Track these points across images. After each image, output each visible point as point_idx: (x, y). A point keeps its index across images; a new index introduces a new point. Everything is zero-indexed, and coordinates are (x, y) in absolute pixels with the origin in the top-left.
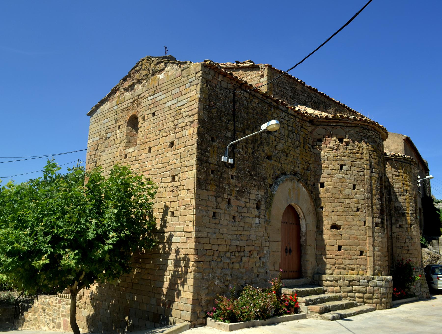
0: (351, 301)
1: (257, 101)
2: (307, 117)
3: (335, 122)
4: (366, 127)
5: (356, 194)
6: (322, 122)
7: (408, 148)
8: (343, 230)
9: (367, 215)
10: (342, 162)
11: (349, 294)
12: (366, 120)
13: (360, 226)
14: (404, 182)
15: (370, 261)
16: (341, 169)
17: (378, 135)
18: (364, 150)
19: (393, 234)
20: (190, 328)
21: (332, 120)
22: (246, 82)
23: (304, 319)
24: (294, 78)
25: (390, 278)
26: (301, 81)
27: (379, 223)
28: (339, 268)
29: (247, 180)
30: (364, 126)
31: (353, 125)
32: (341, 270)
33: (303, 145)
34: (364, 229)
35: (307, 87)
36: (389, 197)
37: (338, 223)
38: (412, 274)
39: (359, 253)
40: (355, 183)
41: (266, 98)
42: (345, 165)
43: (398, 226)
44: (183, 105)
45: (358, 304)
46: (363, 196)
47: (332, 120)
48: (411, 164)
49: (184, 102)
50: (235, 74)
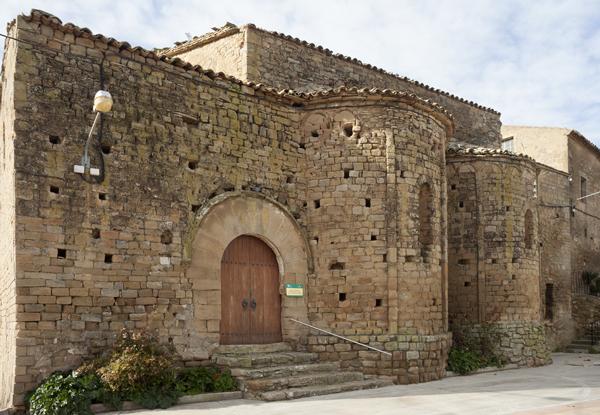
1: (161, 75)
6: (318, 103)
16: (347, 176)
29: (137, 201)
31: (368, 103)
33: (277, 143)
37: (340, 260)
40: (369, 197)
42: (353, 169)
43: (490, 261)
48: (519, 165)
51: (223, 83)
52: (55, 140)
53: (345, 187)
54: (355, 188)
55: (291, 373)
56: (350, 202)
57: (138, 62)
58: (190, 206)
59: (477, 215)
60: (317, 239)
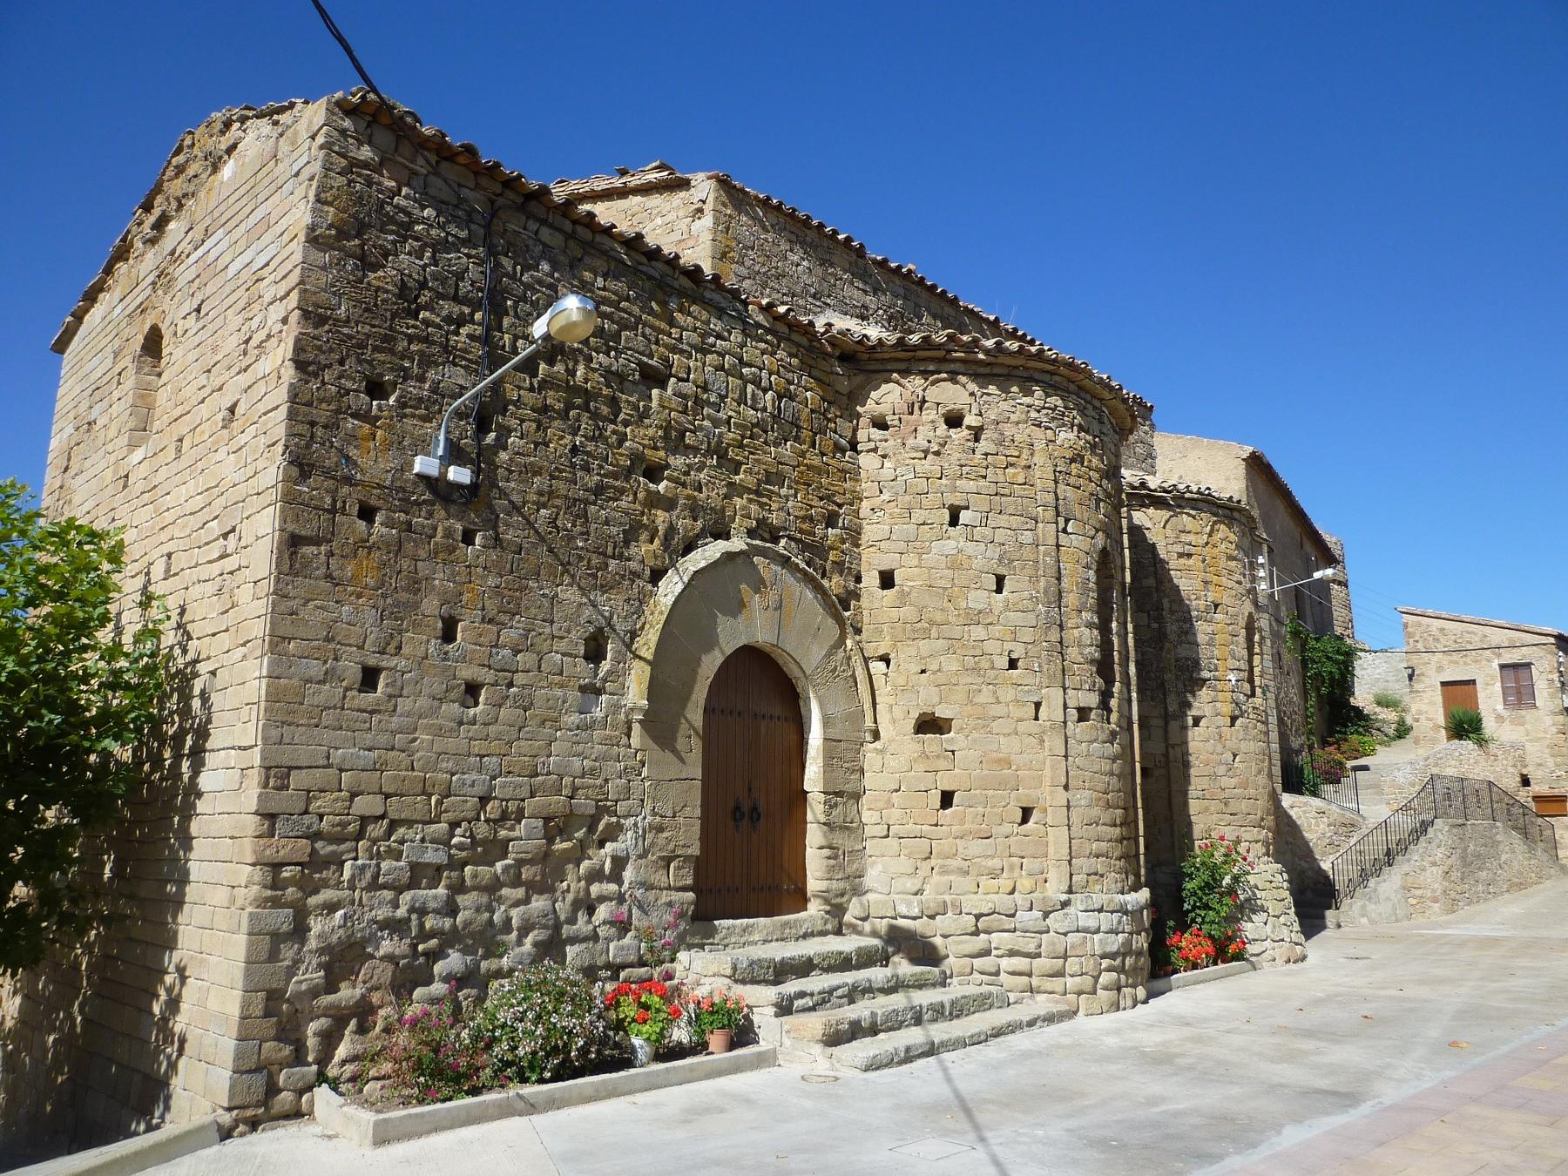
0: (985, 989)
2: (833, 342)
3: (932, 359)
4: (1046, 377)
5: (1007, 608)
6: (890, 360)
7: (1261, 486)
8: (960, 737)
9: (1045, 682)
10: (957, 500)
11: (978, 962)
12: (1041, 351)
13: (1020, 720)
14: (1209, 577)
15: (1057, 841)
16: (954, 521)
17: (1095, 408)
18: (1037, 454)
19: (1171, 751)
20: (222, 1140)
21: (920, 354)
22: (659, 249)
23: (764, 1071)
24: (821, 226)
25: (1144, 895)
26: (848, 240)
27: (1091, 709)
28: (945, 871)
30: (1037, 376)
31: (996, 371)
32: (952, 878)
34: (1035, 730)
35: (875, 261)
36: (1156, 625)
37: (942, 712)
38: (1289, 881)
39: (1019, 815)
40: (1002, 571)
41: (644, 260)
42: (967, 508)
44: (267, 264)
45: (1012, 997)
46: (1031, 616)
47: (920, 354)
49: (272, 250)
50: (604, 212)
51: (717, 297)
52: (376, 389)
53: (950, 546)
54: (970, 548)
55: (869, 990)
56: (962, 578)
57: (559, 230)
58: (648, 572)
59: (1159, 619)
60: (886, 659)
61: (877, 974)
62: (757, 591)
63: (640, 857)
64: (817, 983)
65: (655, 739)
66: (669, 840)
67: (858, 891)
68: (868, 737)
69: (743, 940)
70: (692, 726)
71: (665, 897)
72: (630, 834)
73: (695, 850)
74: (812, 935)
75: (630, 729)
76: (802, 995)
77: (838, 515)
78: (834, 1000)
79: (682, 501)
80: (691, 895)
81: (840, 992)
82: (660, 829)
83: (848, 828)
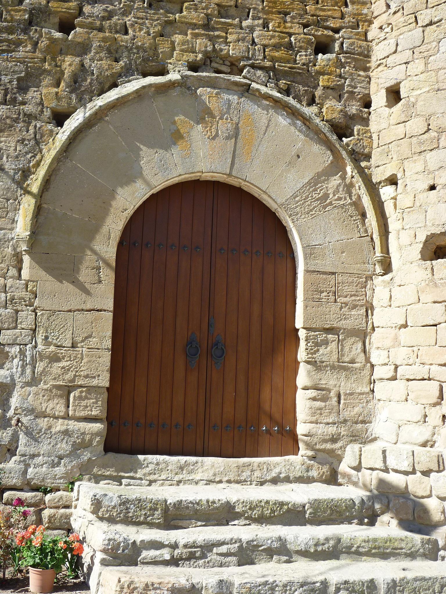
61: (351, 532)
62: (200, 120)
63: (28, 384)
64: (242, 532)
65: (49, 270)
66: (66, 370)
67: (362, 438)
68: (379, 269)
69: (177, 478)
70: (100, 258)
71: (59, 426)
72: (16, 361)
73: (104, 381)
74: (287, 480)
75: (21, 261)
76: (157, 545)
77: (334, 40)
78: (212, 556)
79: (95, 44)
80: (98, 426)
81: (224, 549)
82: (55, 358)
83: (345, 369)
